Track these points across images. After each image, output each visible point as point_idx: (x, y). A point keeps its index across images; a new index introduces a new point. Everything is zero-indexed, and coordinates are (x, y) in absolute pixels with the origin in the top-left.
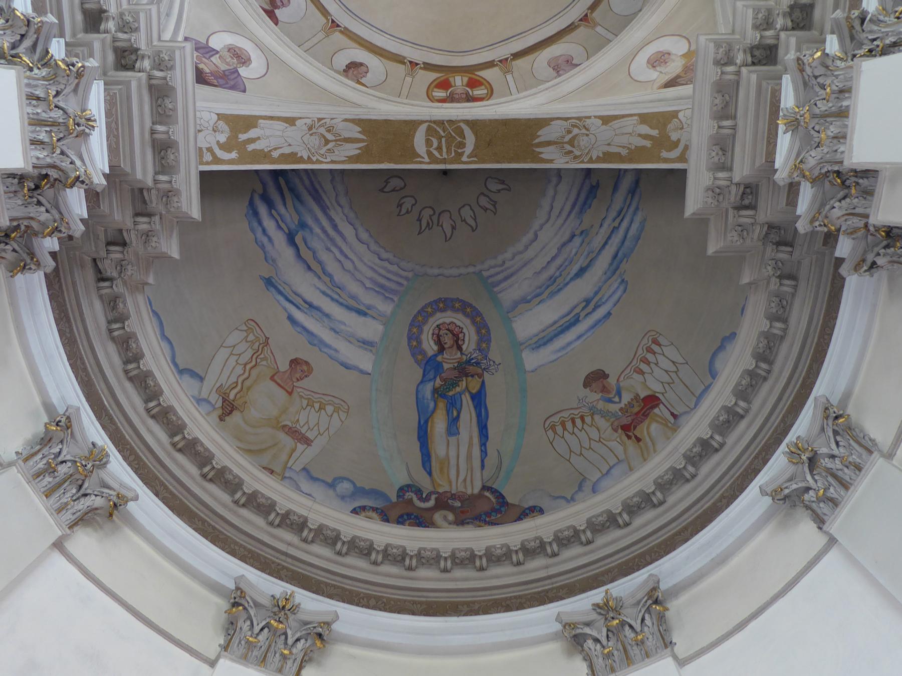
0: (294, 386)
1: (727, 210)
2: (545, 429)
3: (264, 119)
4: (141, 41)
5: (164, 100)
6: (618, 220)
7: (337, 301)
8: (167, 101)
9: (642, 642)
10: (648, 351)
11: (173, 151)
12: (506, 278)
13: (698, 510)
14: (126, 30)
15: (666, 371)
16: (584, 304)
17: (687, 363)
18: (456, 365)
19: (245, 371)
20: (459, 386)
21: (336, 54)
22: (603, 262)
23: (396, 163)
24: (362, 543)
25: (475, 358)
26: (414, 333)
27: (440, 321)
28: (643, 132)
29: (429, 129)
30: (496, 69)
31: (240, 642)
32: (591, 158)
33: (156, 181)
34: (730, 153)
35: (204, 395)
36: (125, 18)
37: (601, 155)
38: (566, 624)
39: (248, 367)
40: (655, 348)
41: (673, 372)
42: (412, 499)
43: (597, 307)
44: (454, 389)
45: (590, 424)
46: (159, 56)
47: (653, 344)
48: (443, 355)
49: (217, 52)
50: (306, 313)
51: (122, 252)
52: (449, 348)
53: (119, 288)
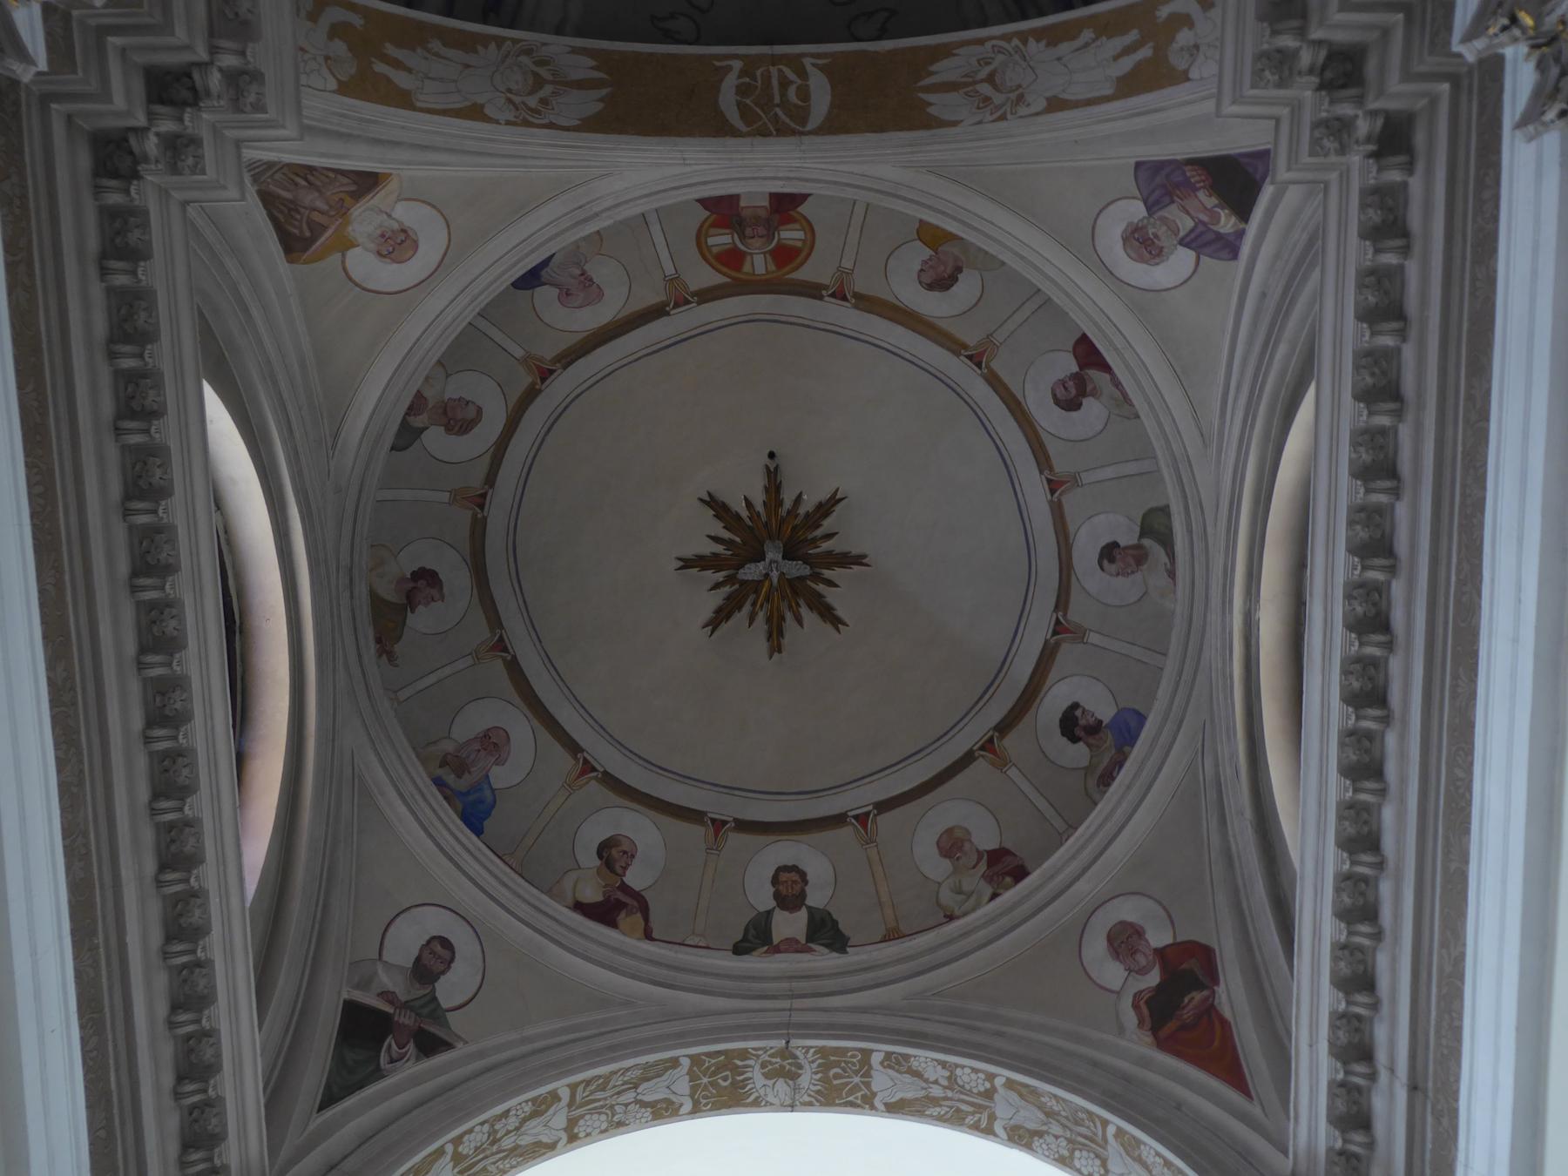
21: (974, 302)
23: (864, 53)
29: (803, 120)
30: (694, 286)
32: (499, 47)
36: (1336, 145)
37: (480, 48)
46: (1281, 78)
49: (1182, 243)
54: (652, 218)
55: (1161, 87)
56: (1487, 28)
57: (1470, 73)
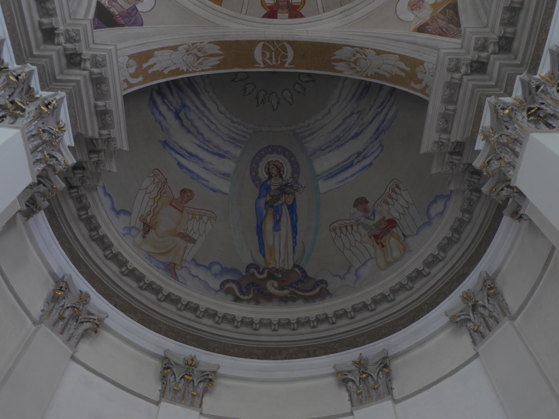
0: (184, 207)
1: (445, 153)
2: (330, 230)
3: (157, 50)
5: (101, 86)
6: (382, 107)
7: (207, 150)
8: (103, 86)
9: (377, 388)
10: (392, 191)
11: (110, 115)
12: (310, 135)
13: (412, 307)
14: (72, 41)
15: (402, 206)
16: (357, 155)
17: (414, 204)
18: (279, 187)
19: (154, 203)
20: (280, 200)
22: (369, 132)
24: (229, 317)
25: (290, 183)
26: (254, 167)
27: (270, 160)
28: (401, 67)
29: (264, 46)
31: (170, 389)
32: (367, 74)
33: (100, 135)
34: (451, 123)
35: (133, 224)
37: (373, 74)
38: (339, 372)
39: (156, 199)
40: (396, 190)
41: (406, 208)
42: (254, 273)
43: (364, 158)
44: (277, 202)
45: (356, 231)
46: (96, 58)
47: (396, 188)
48: (271, 180)
50: (188, 160)
51: (83, 173)
52: (275, 176)
53: (82, 191)
54: (321, 10)
55: (137, 53)
56: (26, 75)
57: (27, 58)
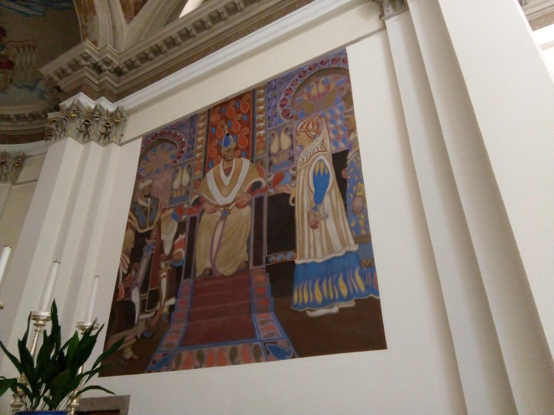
4: (117, 63)
